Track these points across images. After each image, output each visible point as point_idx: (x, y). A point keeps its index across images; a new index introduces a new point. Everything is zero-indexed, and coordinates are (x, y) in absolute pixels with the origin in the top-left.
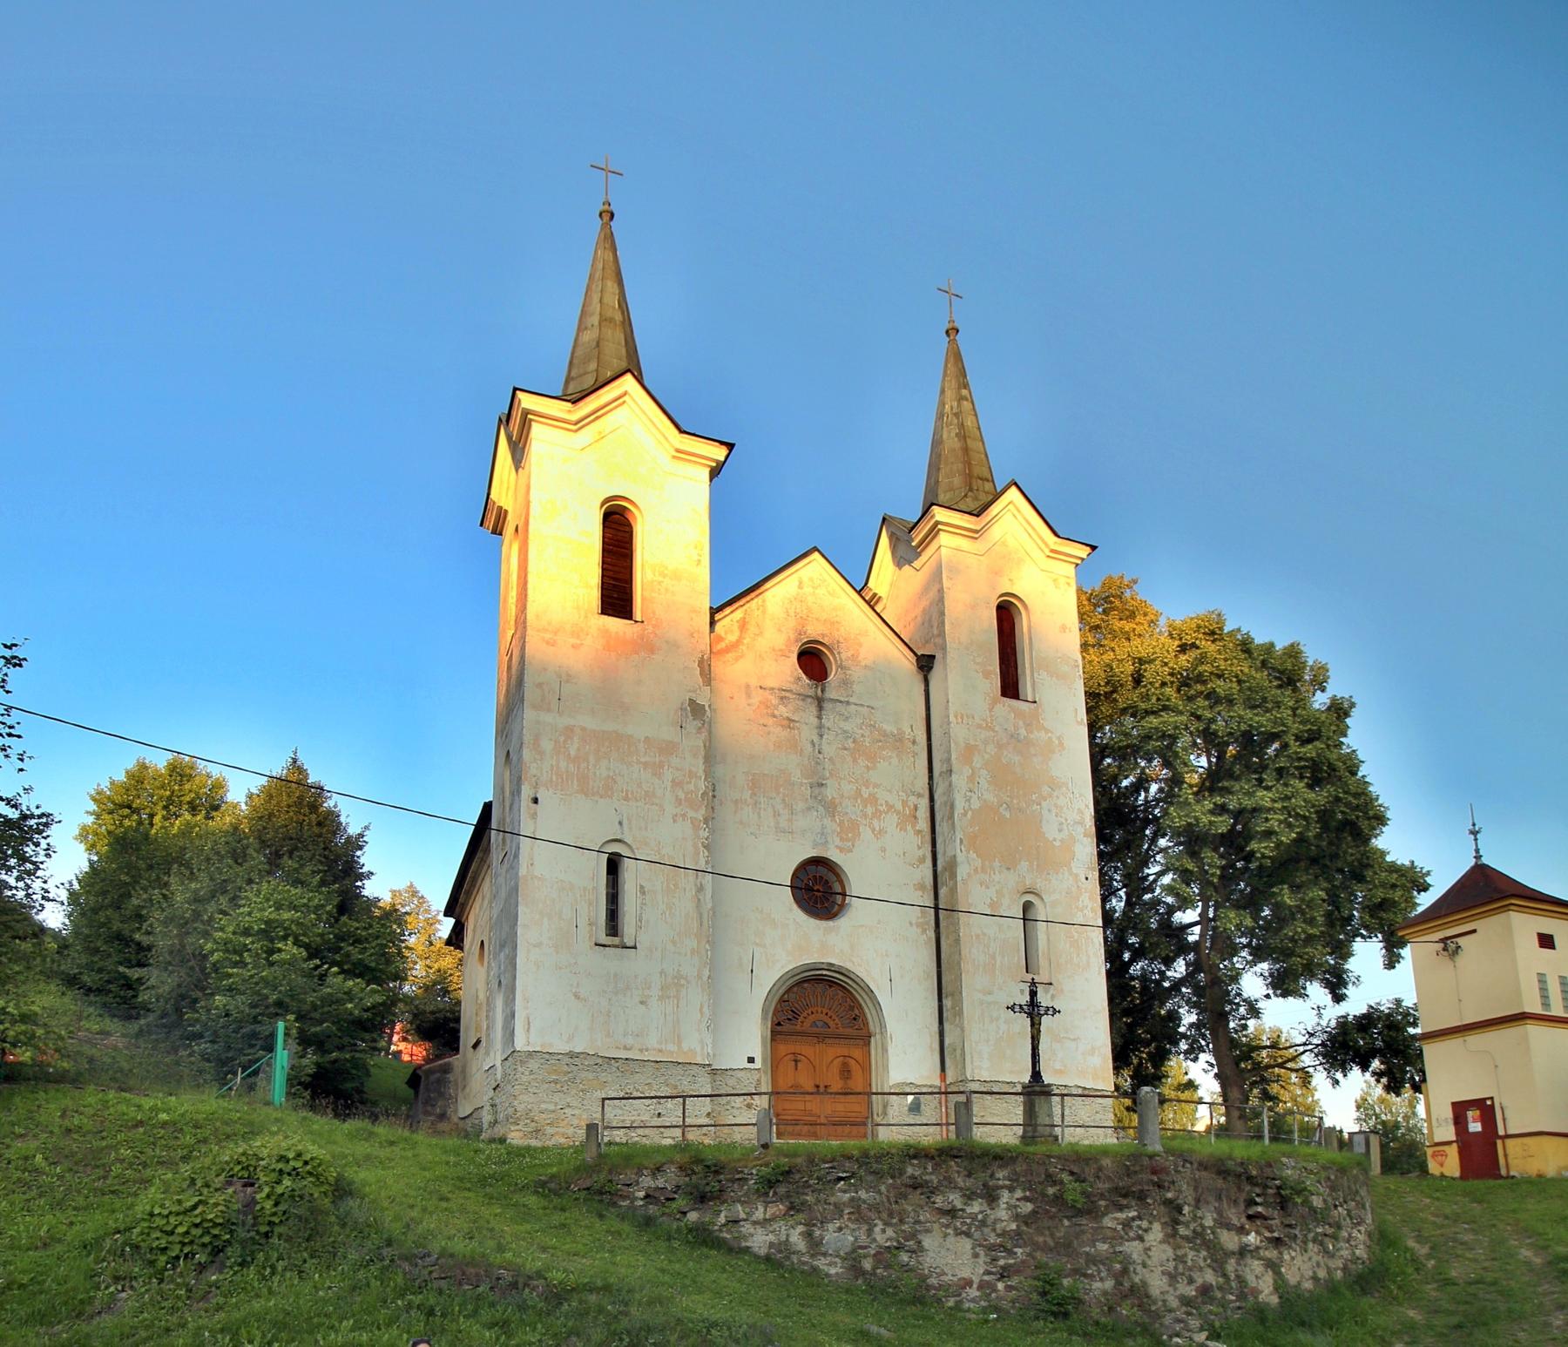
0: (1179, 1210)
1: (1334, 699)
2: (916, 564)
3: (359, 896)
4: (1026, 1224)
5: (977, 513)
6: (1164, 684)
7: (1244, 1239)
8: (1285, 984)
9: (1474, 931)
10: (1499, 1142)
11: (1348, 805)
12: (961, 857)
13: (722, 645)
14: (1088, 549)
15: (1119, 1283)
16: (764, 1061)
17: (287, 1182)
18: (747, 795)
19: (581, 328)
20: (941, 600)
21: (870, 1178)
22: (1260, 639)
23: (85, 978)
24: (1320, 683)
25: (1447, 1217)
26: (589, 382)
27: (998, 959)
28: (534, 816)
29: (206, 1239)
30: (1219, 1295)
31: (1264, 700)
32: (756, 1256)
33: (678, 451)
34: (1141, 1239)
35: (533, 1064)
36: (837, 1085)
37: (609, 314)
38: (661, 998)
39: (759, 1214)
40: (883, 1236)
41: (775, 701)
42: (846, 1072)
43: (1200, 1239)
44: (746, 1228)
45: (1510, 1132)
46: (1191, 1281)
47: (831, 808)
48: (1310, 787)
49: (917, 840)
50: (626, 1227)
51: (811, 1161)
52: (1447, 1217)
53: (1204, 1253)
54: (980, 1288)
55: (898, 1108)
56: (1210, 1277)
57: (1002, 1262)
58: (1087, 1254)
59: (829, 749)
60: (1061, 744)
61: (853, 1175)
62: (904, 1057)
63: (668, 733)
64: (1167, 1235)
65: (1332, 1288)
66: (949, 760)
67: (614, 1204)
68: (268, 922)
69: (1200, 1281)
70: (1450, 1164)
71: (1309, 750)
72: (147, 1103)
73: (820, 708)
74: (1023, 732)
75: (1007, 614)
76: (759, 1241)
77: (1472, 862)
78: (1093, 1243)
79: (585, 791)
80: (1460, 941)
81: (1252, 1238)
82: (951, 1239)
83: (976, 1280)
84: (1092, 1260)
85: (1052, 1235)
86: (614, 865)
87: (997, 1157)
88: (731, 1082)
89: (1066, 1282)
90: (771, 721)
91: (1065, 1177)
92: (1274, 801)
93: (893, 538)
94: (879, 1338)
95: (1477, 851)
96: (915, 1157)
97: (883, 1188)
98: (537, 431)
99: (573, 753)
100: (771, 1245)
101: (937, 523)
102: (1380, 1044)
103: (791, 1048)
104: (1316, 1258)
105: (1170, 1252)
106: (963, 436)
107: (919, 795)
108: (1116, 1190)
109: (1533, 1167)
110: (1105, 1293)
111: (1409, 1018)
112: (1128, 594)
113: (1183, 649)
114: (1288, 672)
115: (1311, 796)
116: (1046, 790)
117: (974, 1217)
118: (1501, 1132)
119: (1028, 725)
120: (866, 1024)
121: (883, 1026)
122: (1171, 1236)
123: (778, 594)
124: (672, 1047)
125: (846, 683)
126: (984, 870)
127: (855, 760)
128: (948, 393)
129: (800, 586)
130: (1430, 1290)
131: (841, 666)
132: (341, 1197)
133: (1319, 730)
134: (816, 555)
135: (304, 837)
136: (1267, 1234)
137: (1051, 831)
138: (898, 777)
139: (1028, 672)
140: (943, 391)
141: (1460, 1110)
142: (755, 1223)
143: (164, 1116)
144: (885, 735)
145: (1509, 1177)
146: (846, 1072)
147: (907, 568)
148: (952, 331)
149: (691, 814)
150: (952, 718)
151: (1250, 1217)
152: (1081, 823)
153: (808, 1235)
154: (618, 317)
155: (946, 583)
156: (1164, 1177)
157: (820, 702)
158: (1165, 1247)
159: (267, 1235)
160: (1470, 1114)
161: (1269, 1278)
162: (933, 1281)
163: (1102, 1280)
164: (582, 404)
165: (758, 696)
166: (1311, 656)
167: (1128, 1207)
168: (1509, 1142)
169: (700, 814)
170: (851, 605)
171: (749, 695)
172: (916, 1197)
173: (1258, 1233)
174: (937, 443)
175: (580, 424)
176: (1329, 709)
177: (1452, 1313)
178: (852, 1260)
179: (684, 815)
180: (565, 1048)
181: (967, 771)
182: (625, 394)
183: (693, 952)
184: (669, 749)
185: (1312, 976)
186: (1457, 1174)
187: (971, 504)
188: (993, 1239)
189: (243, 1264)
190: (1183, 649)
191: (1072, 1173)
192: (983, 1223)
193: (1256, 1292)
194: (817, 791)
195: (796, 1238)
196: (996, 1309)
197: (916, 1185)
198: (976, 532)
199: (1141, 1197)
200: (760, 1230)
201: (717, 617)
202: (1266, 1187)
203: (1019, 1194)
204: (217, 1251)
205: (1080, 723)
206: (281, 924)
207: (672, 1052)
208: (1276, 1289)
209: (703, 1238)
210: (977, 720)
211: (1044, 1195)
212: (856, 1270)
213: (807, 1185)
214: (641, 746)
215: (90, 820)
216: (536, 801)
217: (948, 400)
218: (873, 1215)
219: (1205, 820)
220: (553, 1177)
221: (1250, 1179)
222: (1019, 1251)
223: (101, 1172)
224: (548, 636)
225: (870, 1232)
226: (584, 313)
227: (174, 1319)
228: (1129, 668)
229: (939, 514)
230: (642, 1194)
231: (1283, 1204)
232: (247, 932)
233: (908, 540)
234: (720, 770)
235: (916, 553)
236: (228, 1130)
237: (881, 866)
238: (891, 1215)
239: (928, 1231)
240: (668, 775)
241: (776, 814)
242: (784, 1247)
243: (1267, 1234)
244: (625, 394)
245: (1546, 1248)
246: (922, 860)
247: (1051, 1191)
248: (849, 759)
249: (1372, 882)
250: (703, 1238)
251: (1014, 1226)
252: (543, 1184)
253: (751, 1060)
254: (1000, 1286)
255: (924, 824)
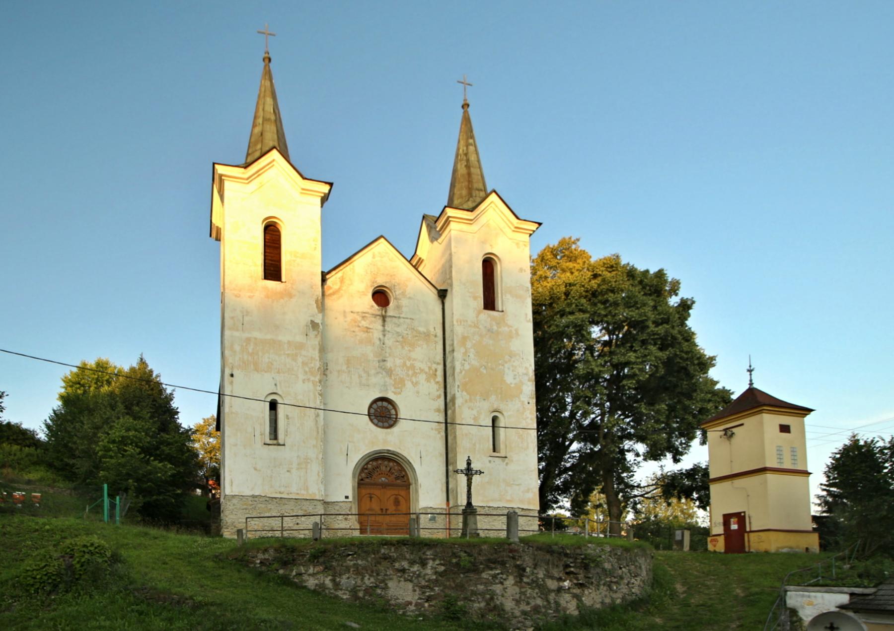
0: (524, 570)
1: (682, 299)
2: (440, 240)
3: (175, 422)
4: (441, 576)
5: (472, 210)
6: (580, 297)
7: (561, 584)
8: (654, 454)
9: (742, 425)
10: (746, 535)
11: (681, 358)
12: (458, 395)
13: (331, 291)
14: (537, 225)
15: (488, 604)
16: (354, 497)
17: (87, 556)
18: (344, 368)
19: (254, 126)
20: (450, 260)
21: (363, 554)
22: (641, 267)
23: (55, 464)
24: (674, 291)
25: (704, 573)
26: (258, 154)
27: (477, 446)
28: (232, 383)
29: (50, 581)
30: (543, 610)
31: (636, 303)
32: (309, 590)
33: (303, 189)
34: (502, 583)
35: (235, 501)
36: (392, 509)
37: (268, 116)
38: (298, 469)
39: (311, 571)
40: (369, 581)
41: (359, 319)
42: (397, 502)
43: (535, 584)
44: (305, 577)
45: (753, 529)
46: (528, 604)
47: (389, 372)
48: (661, 349)
49: (436, 387)
50: (249, 576)
51: (336, 547)
52: (704, 573)
53: (537, 590)
54: (416, 605)
55: (424, 520)
56: (539, 602)
57: (427, 594)
58: (472, 591)
59: (389, 341)
60: (517, 334)
61: (355, 553)
62: (428, 495)
63: (300, 338)
64: (516, 582)
65: (613, 608)
66: (453, 345)
67: (247, 566)
68: (123, 437)
69: (533, 604)
70: (720, 546)
71: (661, 330)
72: (41, 521)
73: (384, 321)
74: (495, 328)
75: (488, 265)
76: (311, 583)
77: (747, 387)
78: (476, 585)
79: (257, 370)
80: (734, 430)
81: (566, 584)
82: (402, 583)
83: (414, 602)
84: (474, 593)
85: (454, 581)
86: (273, 406)
87: (426, 545)
88: (337, 508)
89: (459, 603)
90: (357, 329)
91: (463, 554)
92: (637, 358)
93: (430, 229)
94: (352, 628)
95: (751, 380)
96: (385, 544)
97: (369, 559)
98: (228, 185)
99: (250, 351)
100: (316, 585)
101: (449, 217)
102: (694, 485)
103: (368, 491)
104: (604, 593)
105: (517, 590)
106: (468, 167)
107: (438, 364)
108: (489, 561)
109: (762, 547)
110: (480, 609)
111: (706, 472)
112: (574, 247)
113: (595, 276)
114: (656, 286)
115: (660, 354)
116: (507, 358)
117: (414, 573)
118: (748, 529)
119: (498, 324)
120: (408, 479)
121: (416, 480)
122: (519, 581)
123: (361, 263)
124: (303, 492)
125: (398, 307)
126: (471, 400)
127: (403, 347)
128: (462, 142)
129: (374, 257)
130: (675, 610)
131: (396, 299)
132: (115, 563)
133: (668, 319)
134: (382, 240)
135: (145, 398)
136: (575, 581)
137: (509, 379)
138: (427, 355)
139: (500, 295)
140: (459, 142)
141: (727, 518)
142: (309, 575)
143: (47, 527)
144: (420, 333)
145: (749, 552)
146: (397, 502)
147: (435, 242)
148: (465, 106)
149: (312, 378)
150: (455, 323)
151: (567, 573)
152: (526, 374)
153: (333, 581)
154: (273, 118)
155: (453, 250)
156: (516, 554)
157: (384, 318)
158: (515, 587)
159: (77, 579)
160: (732, 520)
161: (574, 603)
162: (393, 602)
163: (479, 602)
164: (250, 168)
165: (350, 317)
166: (670, 276)
167: (496, 568)
168: (752, 535)
169: (317, 379)
170: (402, 265)
171: (345, 316)
172: (385, 563)
173: (570, 581)
174: (455, 171)
175: (249, 179)
176: (679, 305)
177: (678, 620)
178: (354, 591)
179: (309, 379)
180: (251, 493)
181: (463, 350)
182: (274, 160)
183: (314, 446)
184: (301, 346)
185: (670, 452)
186: (723, 551)
187: (470, 204)
188: (423, 583)
189: (67, 592)
190: (595, 276)
191: (465, 552)
192: (419, 576)
193: (565, 609)
194: (382, 364)
195: (328, 582)
196: (424, 616)
197: (386, 558)
198: (471, 220)
199: (503, 564)
200: (311, 579)
201: (328, 277)
202: (576, 559)
203: (437, 562)
204: (55, 586)
205: (529, 321)
206: (128, 437)
207: (304, 495)
208: (578, 607)
209: (285, 581)
210: (469, 323)
211: (450, 562)
212: (356, 597)
213: (333, 558)
214: (286, 346)
215: (63, 390)
216: (232, 375)
217: (461, 147)
218: (364, 571)
219: (597, 370)
220: (221, 553)
221: (566, 555)
222: (437, 589)
223: (17, 551)
224: (236, 293)
225: (362, 579)
226: (255, 118)
227: (34, 614)
228: (563, 289)
229: (450, 212)
230: (258, 561)
231: (586, 567)
232: (114, 442)
233: (435, 225)
234: (330, 356)
235: (440, 233)
236: (76, 532)
237: (417, 402)
238: (372, 572)
239: (391, 579)
240: (300, 360)
241: (360, 377)
242: (322, 586)
243: (575, 581)
244: (274, 160)
245: (748, 589)
246: (439, 397)
247: (454, 561)
248: (400, 347)
249: (696, 399)
250: (285, 581)
251: (434, 577)
252: (216, 557)
253: (347, 497)
254: (426, 605)
255: (440, 378)
